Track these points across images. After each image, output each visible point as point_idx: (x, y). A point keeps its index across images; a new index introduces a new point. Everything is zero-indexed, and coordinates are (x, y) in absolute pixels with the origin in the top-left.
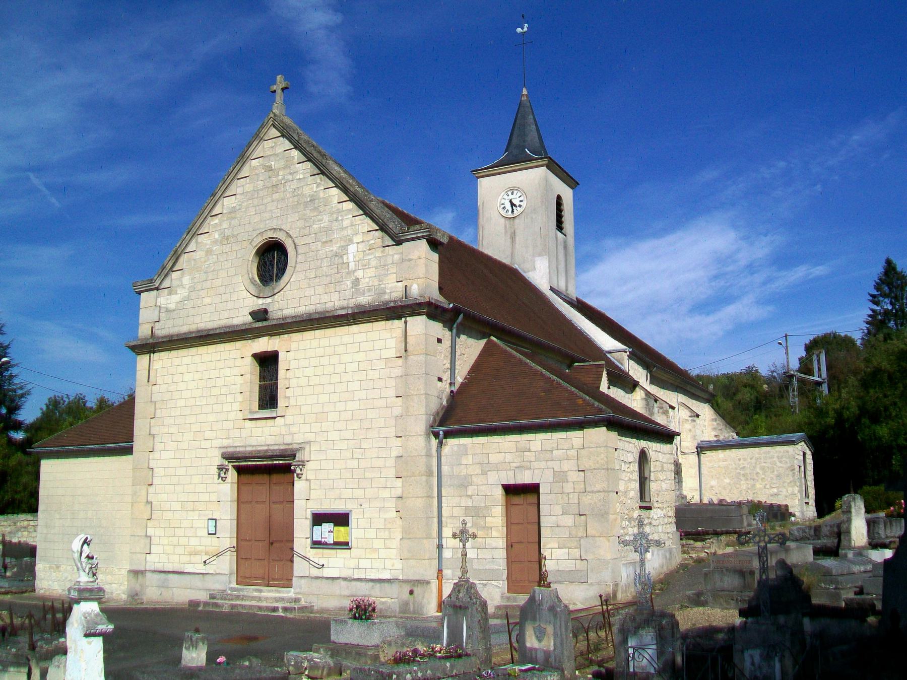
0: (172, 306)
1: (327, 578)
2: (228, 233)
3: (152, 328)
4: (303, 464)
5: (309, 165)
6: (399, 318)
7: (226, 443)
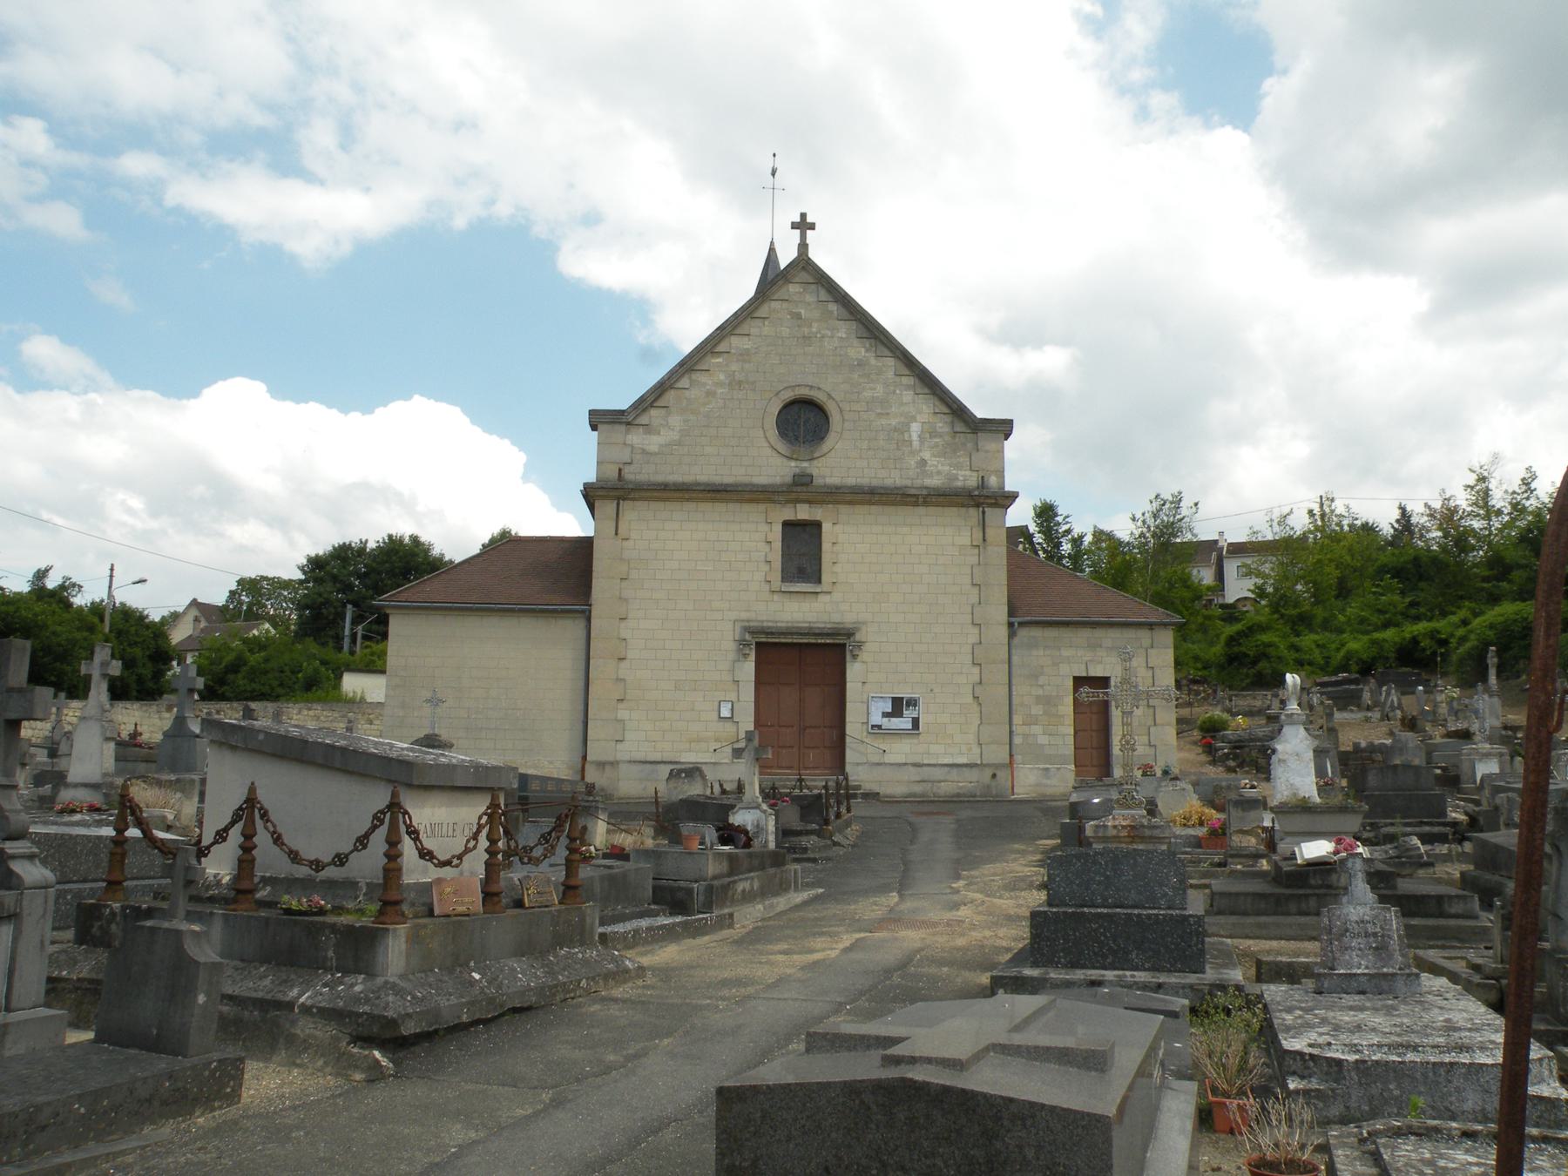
0: (654, 448)
1: (892, 764)
2: (738, 376)
3: (620, 470)
4: (860, 645)
7: (744, 616)
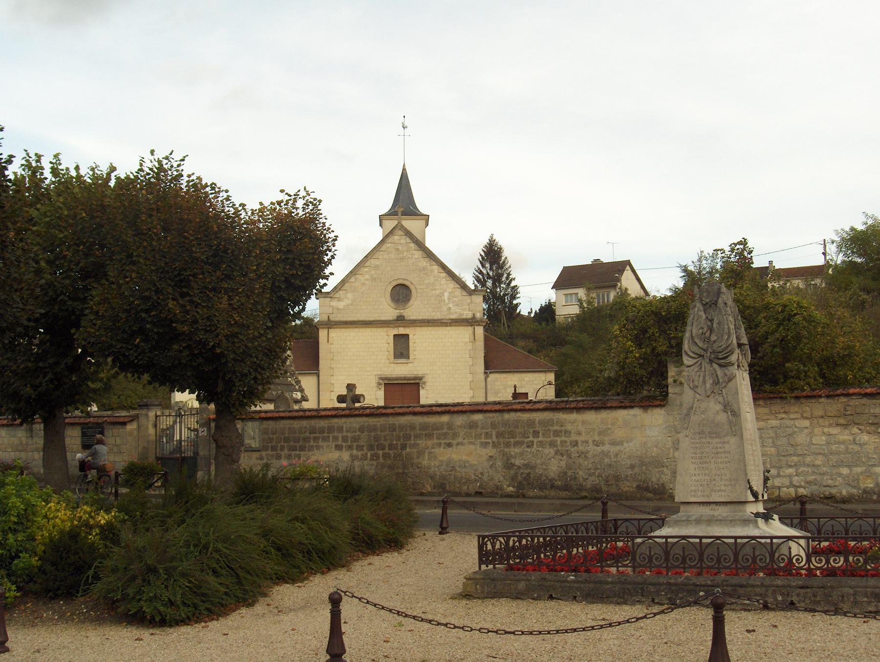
0: (341, 307)
2: (375, 276)
5: (421, 252)
6: (472, 326)
7: (379, 373)
